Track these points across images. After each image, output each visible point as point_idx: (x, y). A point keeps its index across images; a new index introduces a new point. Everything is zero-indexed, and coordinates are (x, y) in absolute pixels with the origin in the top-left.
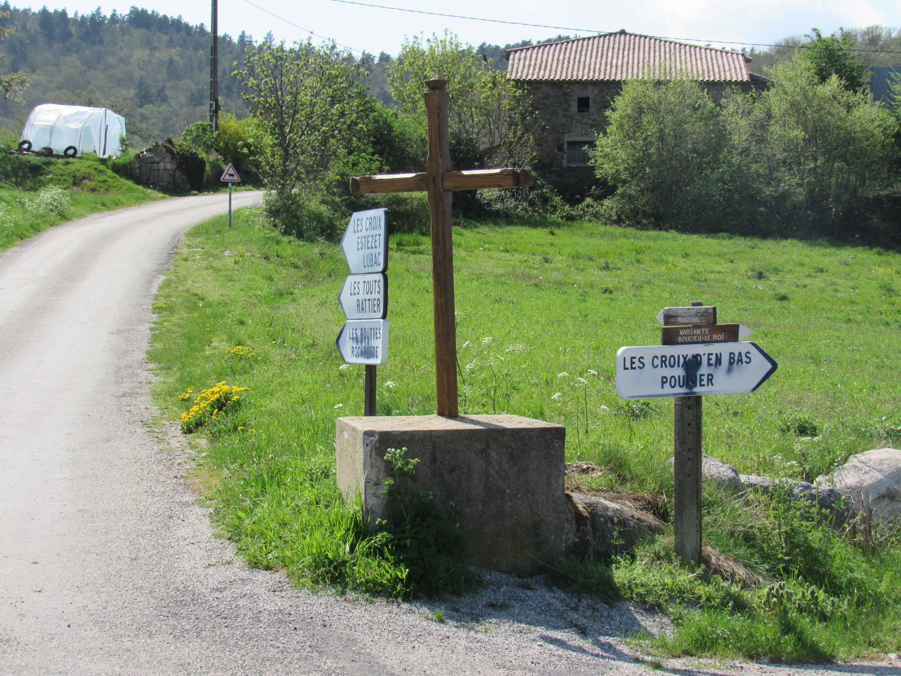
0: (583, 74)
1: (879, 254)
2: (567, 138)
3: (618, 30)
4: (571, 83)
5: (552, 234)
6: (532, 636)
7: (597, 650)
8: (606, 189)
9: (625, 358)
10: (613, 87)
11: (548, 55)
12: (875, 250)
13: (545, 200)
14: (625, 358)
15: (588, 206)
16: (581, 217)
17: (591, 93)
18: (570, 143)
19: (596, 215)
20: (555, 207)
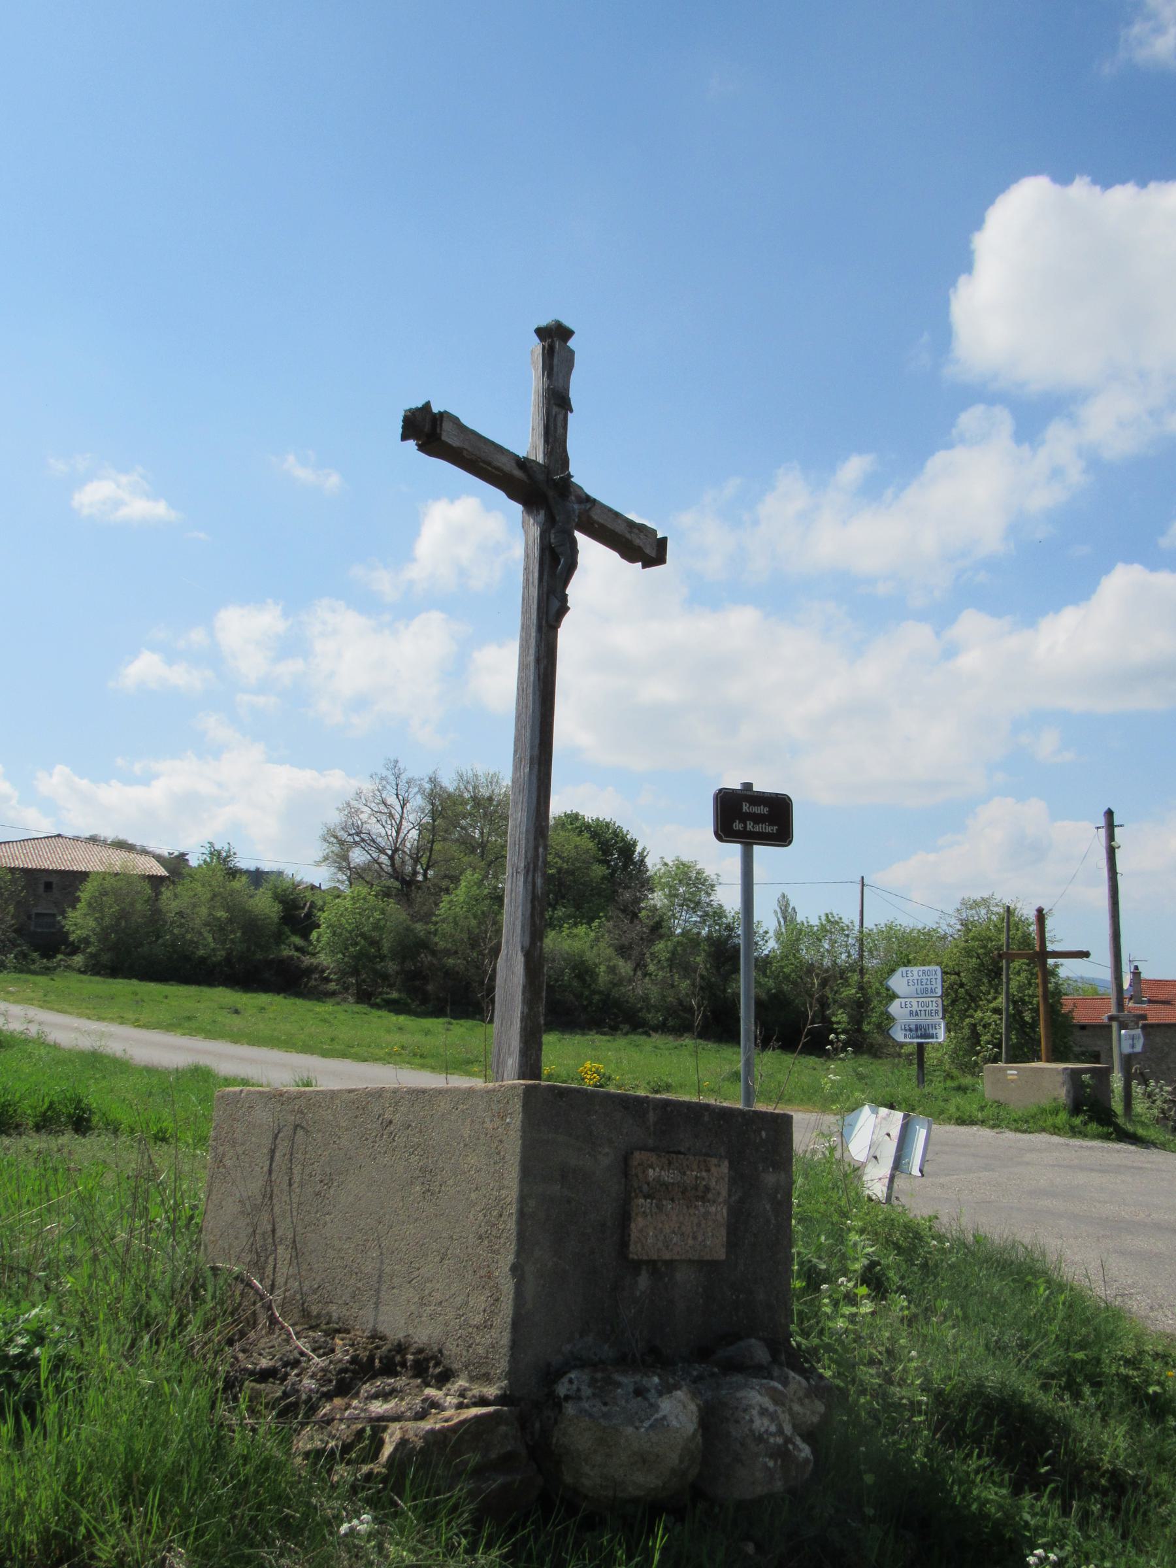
0: (47, 865)
1: (285, 998)
2: (35, 911)
3: (87, 835)
4: (40, 871)
5: (53, 980)
6: (972, 1414)
7: (202, 1462)
8: (74, 950)
9: (1086, 954)
10: (83, 876)
11: (16, 850)
12: (282, 995)
13: (25, 956)
14: (1086, 954)
15: (61, 960)
16: (55, 968)
17: (54, 880)
18: (38, 915)
19: (68, 967)
20: (33, 960)
